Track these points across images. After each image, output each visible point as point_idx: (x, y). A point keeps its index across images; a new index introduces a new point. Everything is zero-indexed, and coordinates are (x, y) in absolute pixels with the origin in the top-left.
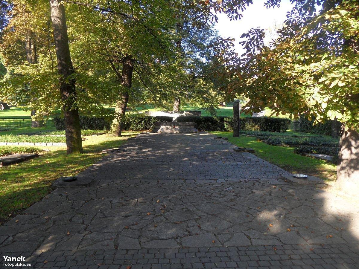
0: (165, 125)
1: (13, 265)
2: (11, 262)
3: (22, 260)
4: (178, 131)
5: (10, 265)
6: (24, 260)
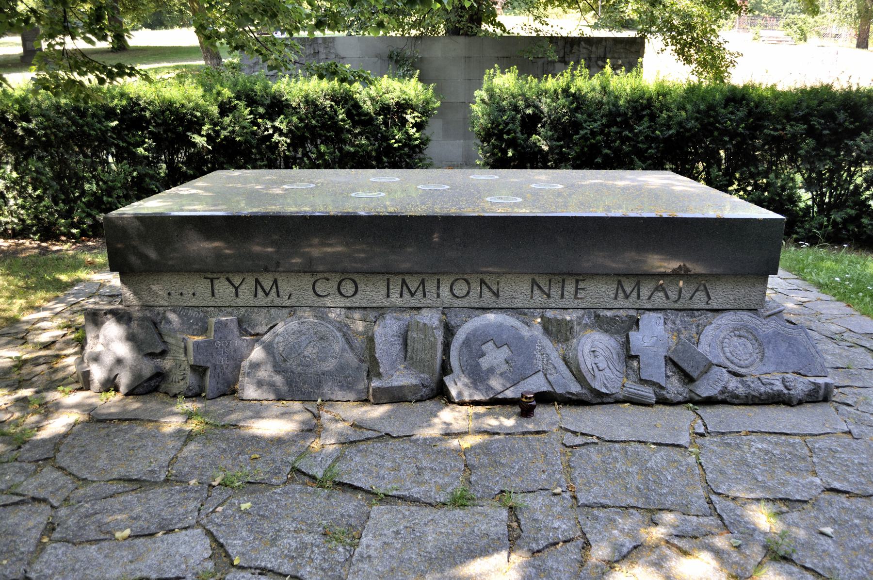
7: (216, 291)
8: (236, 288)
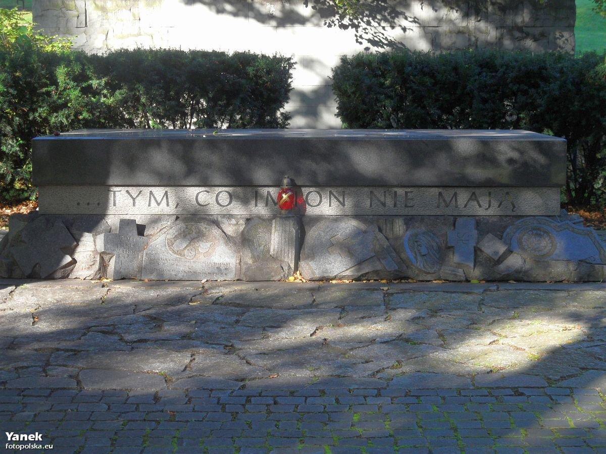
0: (168, 180)
1: (22, 447)
2: (19, 442)
3: (37, 439)
4: (338, 267)
5: (18, 447)
6: (41, 439)
7: (117, 202)
8: (134, 199)
